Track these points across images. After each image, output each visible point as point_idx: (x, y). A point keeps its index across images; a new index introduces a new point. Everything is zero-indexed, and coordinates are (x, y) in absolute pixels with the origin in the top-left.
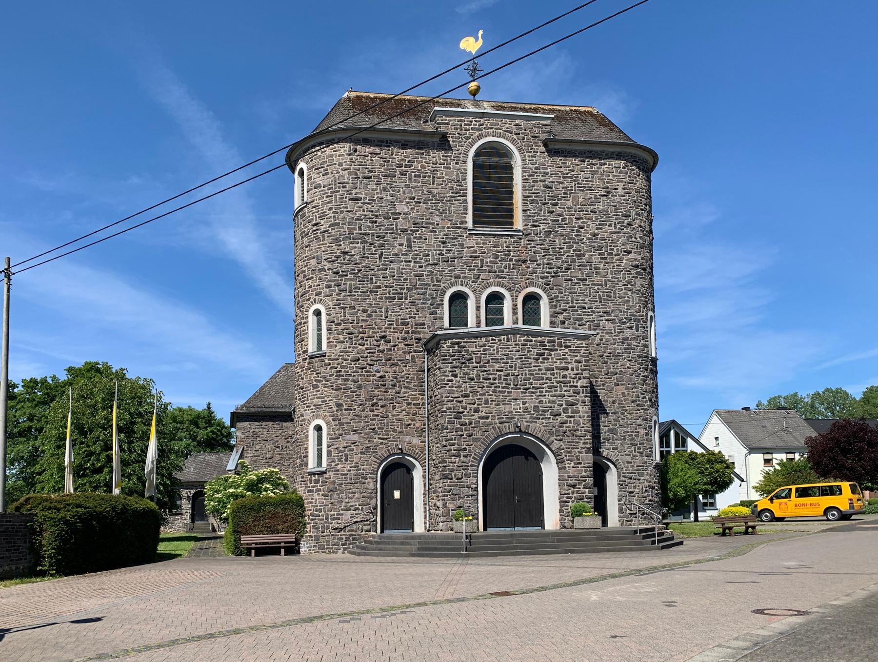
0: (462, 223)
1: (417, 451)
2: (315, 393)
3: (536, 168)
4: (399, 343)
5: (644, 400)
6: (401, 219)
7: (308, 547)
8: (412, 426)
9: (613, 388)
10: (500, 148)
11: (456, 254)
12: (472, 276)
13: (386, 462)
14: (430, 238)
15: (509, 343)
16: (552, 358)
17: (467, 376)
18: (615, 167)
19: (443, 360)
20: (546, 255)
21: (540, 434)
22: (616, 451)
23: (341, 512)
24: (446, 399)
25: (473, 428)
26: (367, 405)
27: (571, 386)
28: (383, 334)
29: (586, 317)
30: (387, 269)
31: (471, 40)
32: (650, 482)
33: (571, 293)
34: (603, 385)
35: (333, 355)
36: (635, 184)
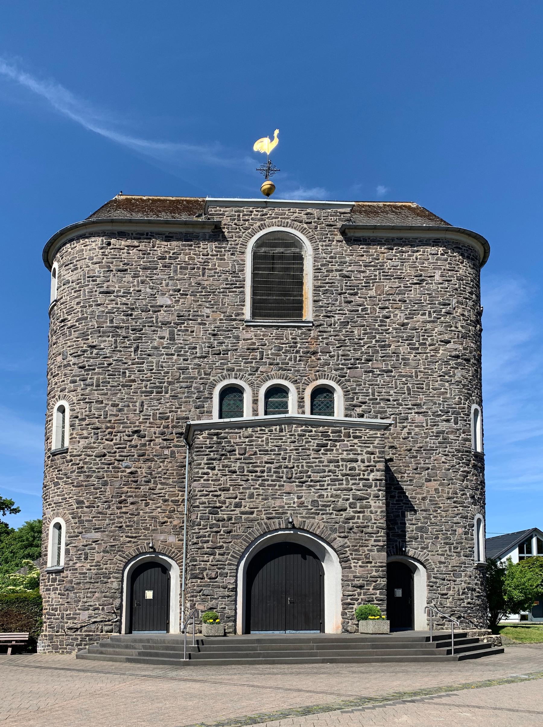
0: (237, 315)
1: (173, 550)
2: (56, 491)
3: (331, 257)
4: (156, 437)
5: (464, 497)
6: (162, 312)
7: (43, 647)
8: (168, 523)
9: (423, 484)
10: (288, 239)
11: (229, 347)
12: (249, 369)
13: (134, 562)
14: (198, 331)
15: (284, 434)
16: (337, 450)
17: (227, 469)
18: (431, 254)
19: (197, 452)
20: (341, 346)
21: (319, 530)
22: (425, 551)
23: (78, 611)
24: (199, 494)
25: (233, 524)
26: (113, 502)
27: (360, 479)
28: (136, 429)
29: (391, 409)
30: (144, 362)
31: (266, 140)
32: (469, 583)
33: (372, 385)
34: (411, 480)
35: (75, 451)
36: (457, 271)
